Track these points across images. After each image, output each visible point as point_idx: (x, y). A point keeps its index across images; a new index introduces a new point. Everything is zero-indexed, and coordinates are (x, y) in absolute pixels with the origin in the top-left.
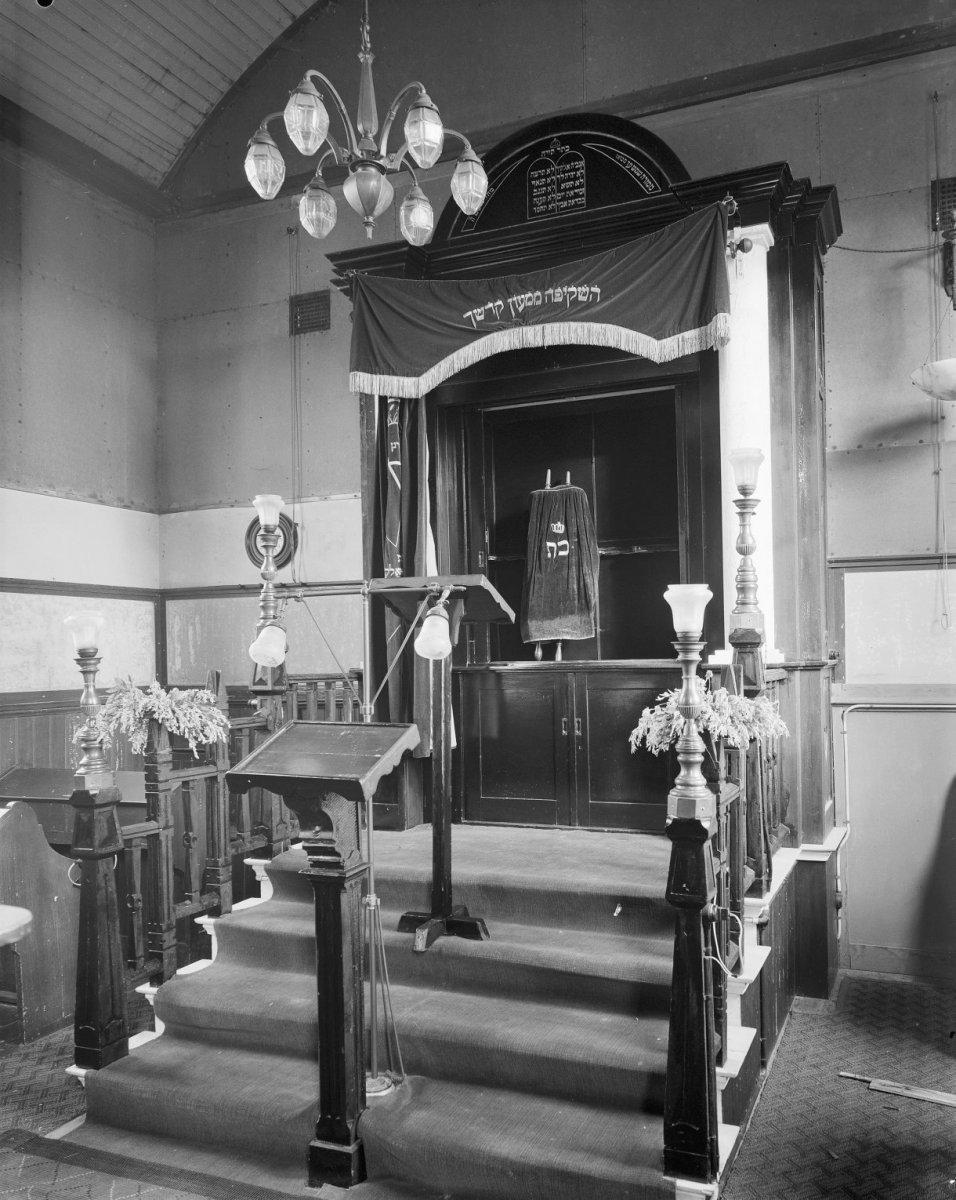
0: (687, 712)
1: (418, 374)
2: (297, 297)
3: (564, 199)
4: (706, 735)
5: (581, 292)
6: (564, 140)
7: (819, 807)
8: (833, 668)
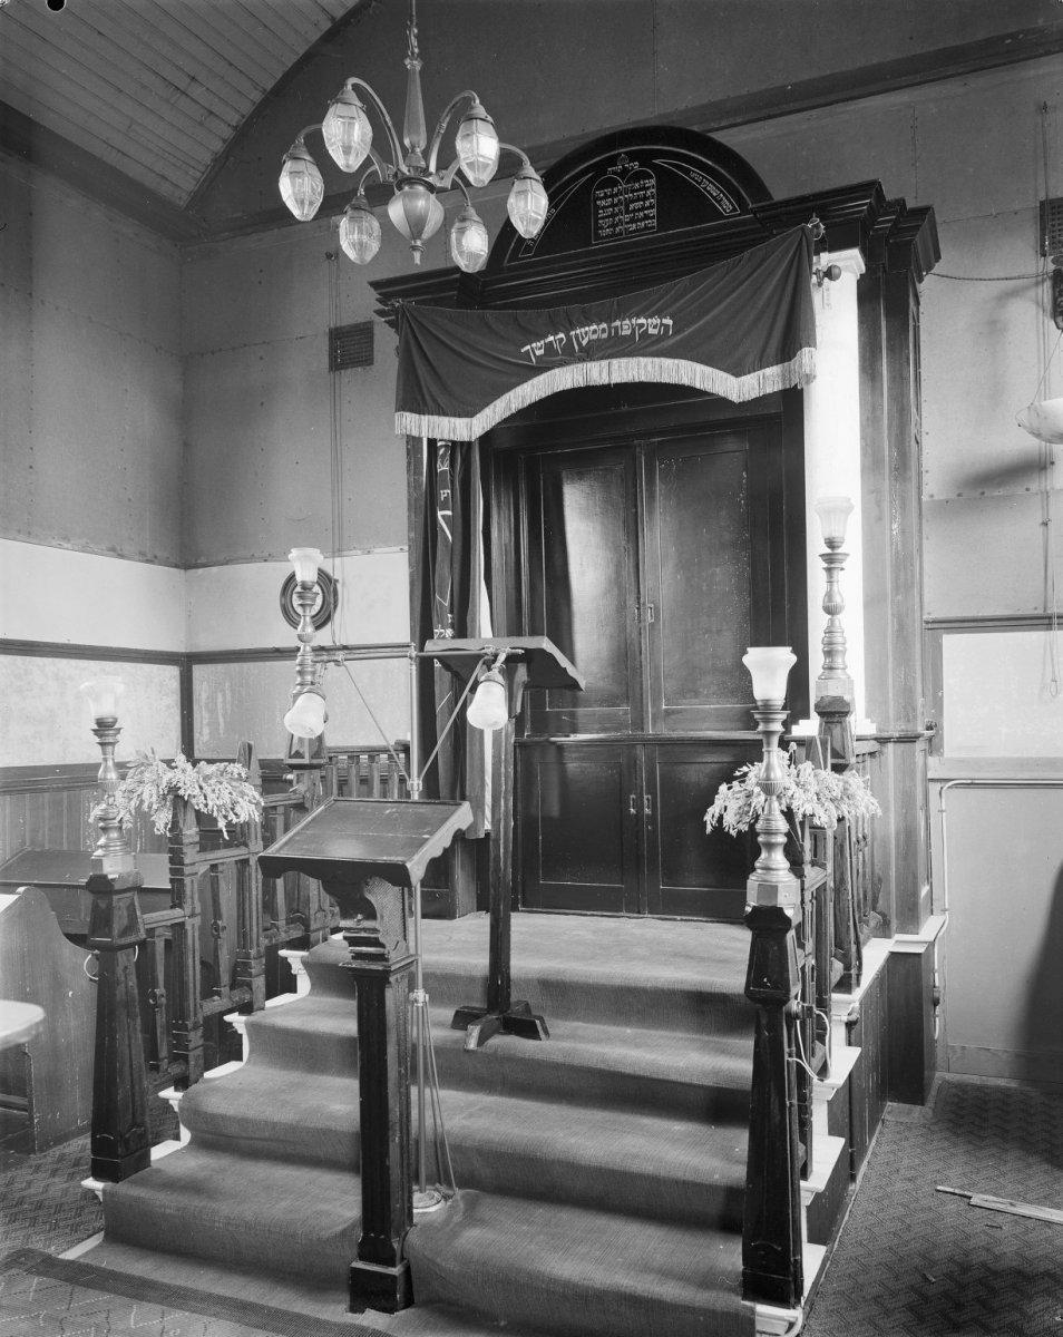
0: (768, 789)
1: (471, 415)
3: (632, 221)
4: (789, 814)
5: (652, 325)
6: (632, 156)
7: (915, 894)
8: (930, 740)
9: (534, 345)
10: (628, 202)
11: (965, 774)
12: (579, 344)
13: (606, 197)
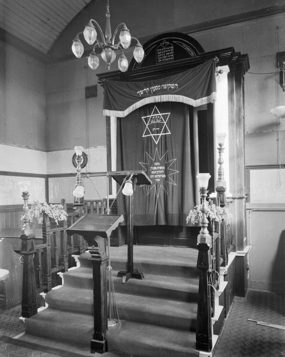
1: (123, 110)
3: (167, 58)
4: (209, 218)
5: (172, 86)
6: (167, 40)
8: (247, 198)
9: (140, 91)
10: (166, 53)
11: (256, 208)
12: (153, 91)
13: (160, 51)
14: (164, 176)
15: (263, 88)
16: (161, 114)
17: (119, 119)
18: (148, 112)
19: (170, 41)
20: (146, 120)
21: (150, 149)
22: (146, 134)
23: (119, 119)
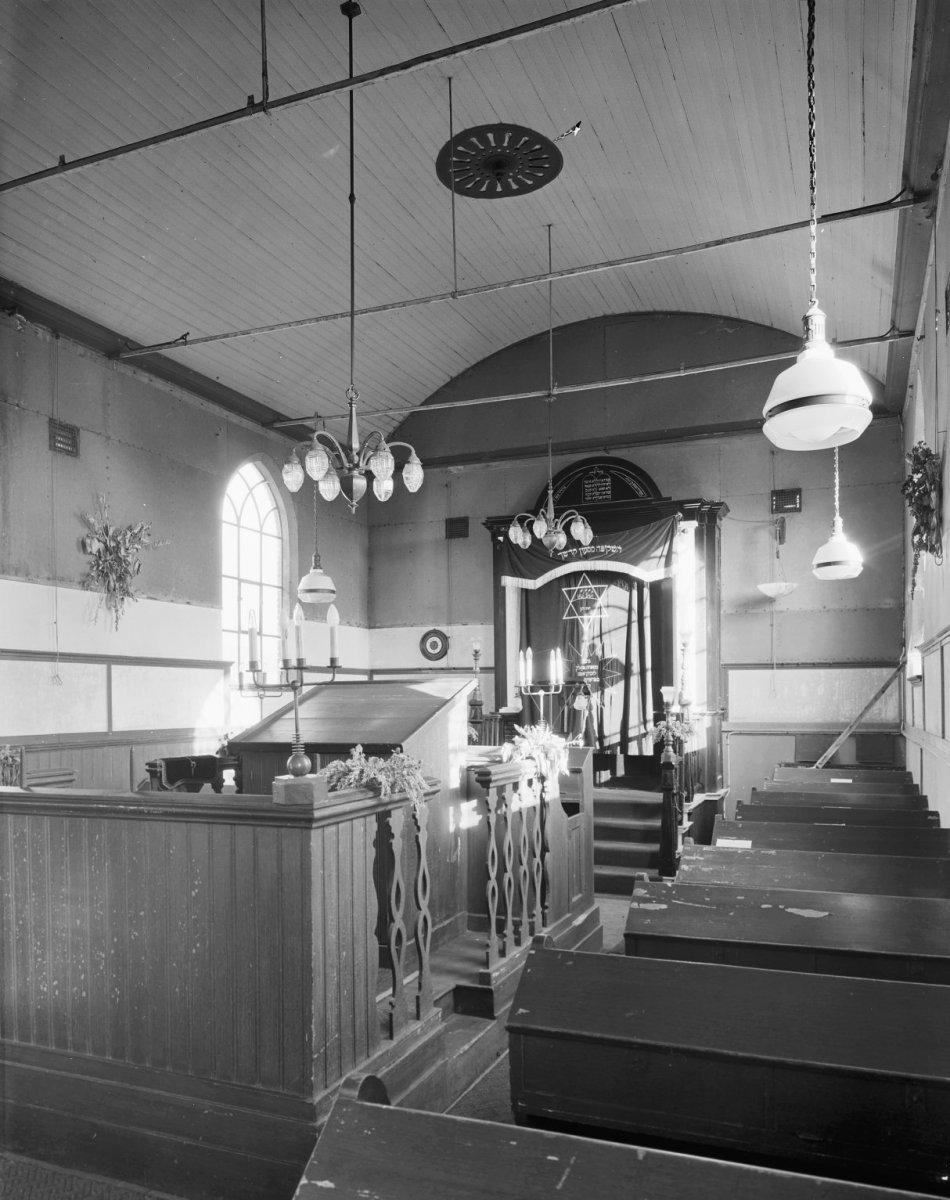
0: (668, 728)
1: (535, 579)
2: (451, 519)
3: (600, 495)
4: (673, 736)
5: (613, 548)
6: (601, 468)
7: (715, 777)
8: (723, 714)
11: (737, 729)
14: (597, 680)
15: (750, 542)
16: (593, 587)
17: (525, 593)
18: (572, 581)
19: (606, 469)
20: (570, 593)
21: (575, 638)
22: (569, 615)
23: (525, 593)
